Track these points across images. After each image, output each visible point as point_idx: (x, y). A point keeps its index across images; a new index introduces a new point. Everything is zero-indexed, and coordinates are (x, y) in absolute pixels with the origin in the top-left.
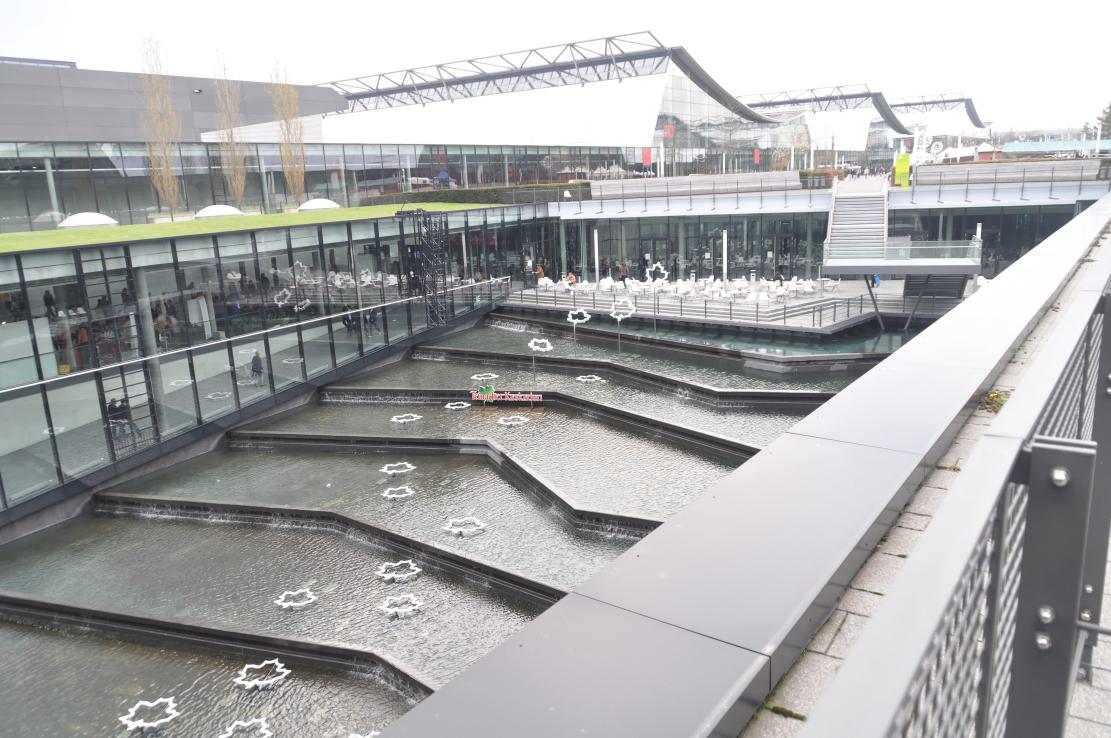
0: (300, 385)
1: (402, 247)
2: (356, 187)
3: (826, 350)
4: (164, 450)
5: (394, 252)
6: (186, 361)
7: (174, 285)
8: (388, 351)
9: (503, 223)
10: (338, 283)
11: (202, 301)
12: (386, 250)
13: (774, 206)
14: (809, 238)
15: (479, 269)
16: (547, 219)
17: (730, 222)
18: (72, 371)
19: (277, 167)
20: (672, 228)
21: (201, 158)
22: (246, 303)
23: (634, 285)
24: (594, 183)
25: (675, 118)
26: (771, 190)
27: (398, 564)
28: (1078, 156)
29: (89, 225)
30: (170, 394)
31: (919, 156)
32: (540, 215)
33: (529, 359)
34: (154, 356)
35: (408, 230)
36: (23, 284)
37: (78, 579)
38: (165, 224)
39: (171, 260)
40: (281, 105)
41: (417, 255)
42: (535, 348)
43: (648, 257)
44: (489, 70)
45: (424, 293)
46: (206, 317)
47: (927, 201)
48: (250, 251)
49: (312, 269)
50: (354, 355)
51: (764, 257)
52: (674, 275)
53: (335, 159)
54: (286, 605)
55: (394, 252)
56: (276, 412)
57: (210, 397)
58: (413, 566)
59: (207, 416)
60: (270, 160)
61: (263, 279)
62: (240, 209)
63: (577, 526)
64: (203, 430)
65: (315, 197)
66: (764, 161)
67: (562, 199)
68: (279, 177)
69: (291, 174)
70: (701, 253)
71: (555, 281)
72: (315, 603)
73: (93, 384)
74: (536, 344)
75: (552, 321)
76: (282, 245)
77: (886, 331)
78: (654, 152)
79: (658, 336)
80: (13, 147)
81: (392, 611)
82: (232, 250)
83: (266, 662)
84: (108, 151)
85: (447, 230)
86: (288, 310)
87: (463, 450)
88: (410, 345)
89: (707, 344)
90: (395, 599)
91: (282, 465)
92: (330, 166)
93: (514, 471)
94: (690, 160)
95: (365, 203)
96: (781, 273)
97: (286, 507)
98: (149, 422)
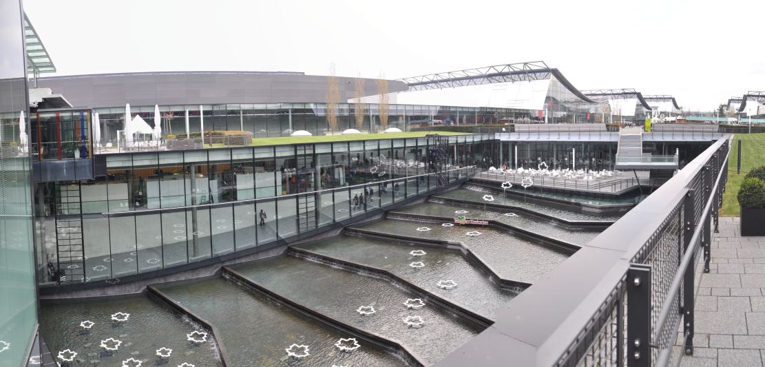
0: (378, 209)
1: (428, 150)
2: (409, 123)
3: (618, 202)
4: (318, 232)
5: (424, 152)
6: (331, 194)
7: (330, 161)
8: (418, 197)
9: (473, 142)
10: (398, 165)
11: (341, 169)
12: (421, 151)
13: (595, 138)
14: (610, 152)
15: (461, 162)
16: (494, 140)
17: (577, 145)
18: (287, 194)
19: (377, 114)
20: (551, 146)
21: (347, 109)
22: (359, 170)
23: (533, 171)
24: (516, 125)
25: (554, 99)
26: (594, 131)
27: (414, 300)
28: (712, 123)
29: (302, 135)
30: (323, 208)
31: (655, 119)
32: (491, 138)
33: (483, 204)
34: (319, 191)
35: (431, 143)
36: (275, 157)
37: (278, 282)
38: (330, 136)
39: (330, 151)
40: (381, 88)
41: (434, 154)
42: (486, 199)
43: (539, 159)
44: (471, 75)
45: (435, 171)
46: (341, 176)
47: (658, 138)
48: (362, 149)
49: (388, 158)
50: (402, 198)
51: (591, 160)
52: (551, 168)
53: (401, 111)
54: (361, 313)
55: (424, 152)
56: (366, 221)
57: (339, 211)
58: (421, 302)
59: (337, 219)
60: (374, 111)
61: (366, 161)
62: (360, 131)
63: (502, 287)
64: (335, 225)
65: (392, 127)
66: (591, 119)
67: (502, 131)
68: (377, 118)
69: (382, 116)
70: (563, 158)
71: (497, 168)
72: (374, 314)
73: (295, 200)
74: (486, 197)
75: (494, 187)
76: (375, 147)
77: (642, 194)
78: (543, 112)
79: (543, 195)
80: (279, 105)
81: (409, 324)
82: (355, 148)
83: (350, 339)
84: (312, 106)
85: (448, 144)
86: (376, 175)
87: (449, 247)
88: (427, 195)
89: (566, 199)
90: (412, 317)
91: (366, 246)
92: (399, 114)
93: (473, 259)
94: (560, 116)
95: (413, 130)
96: (598, 168)
97: (366, 265)
98: (314, 219)
